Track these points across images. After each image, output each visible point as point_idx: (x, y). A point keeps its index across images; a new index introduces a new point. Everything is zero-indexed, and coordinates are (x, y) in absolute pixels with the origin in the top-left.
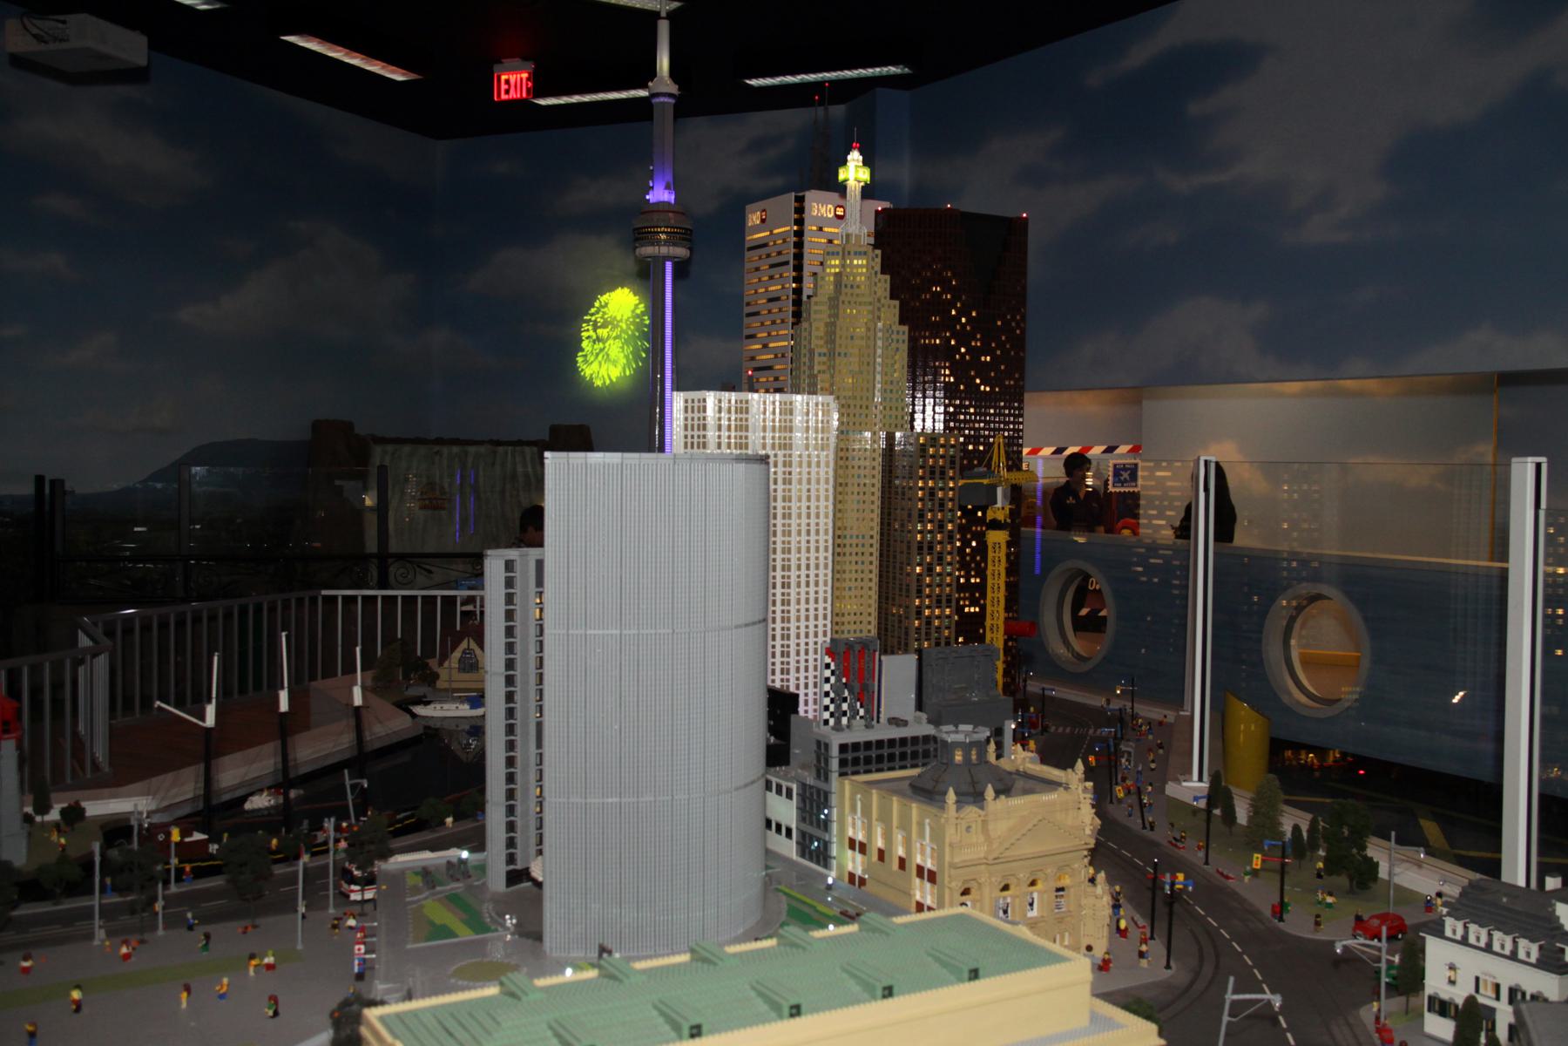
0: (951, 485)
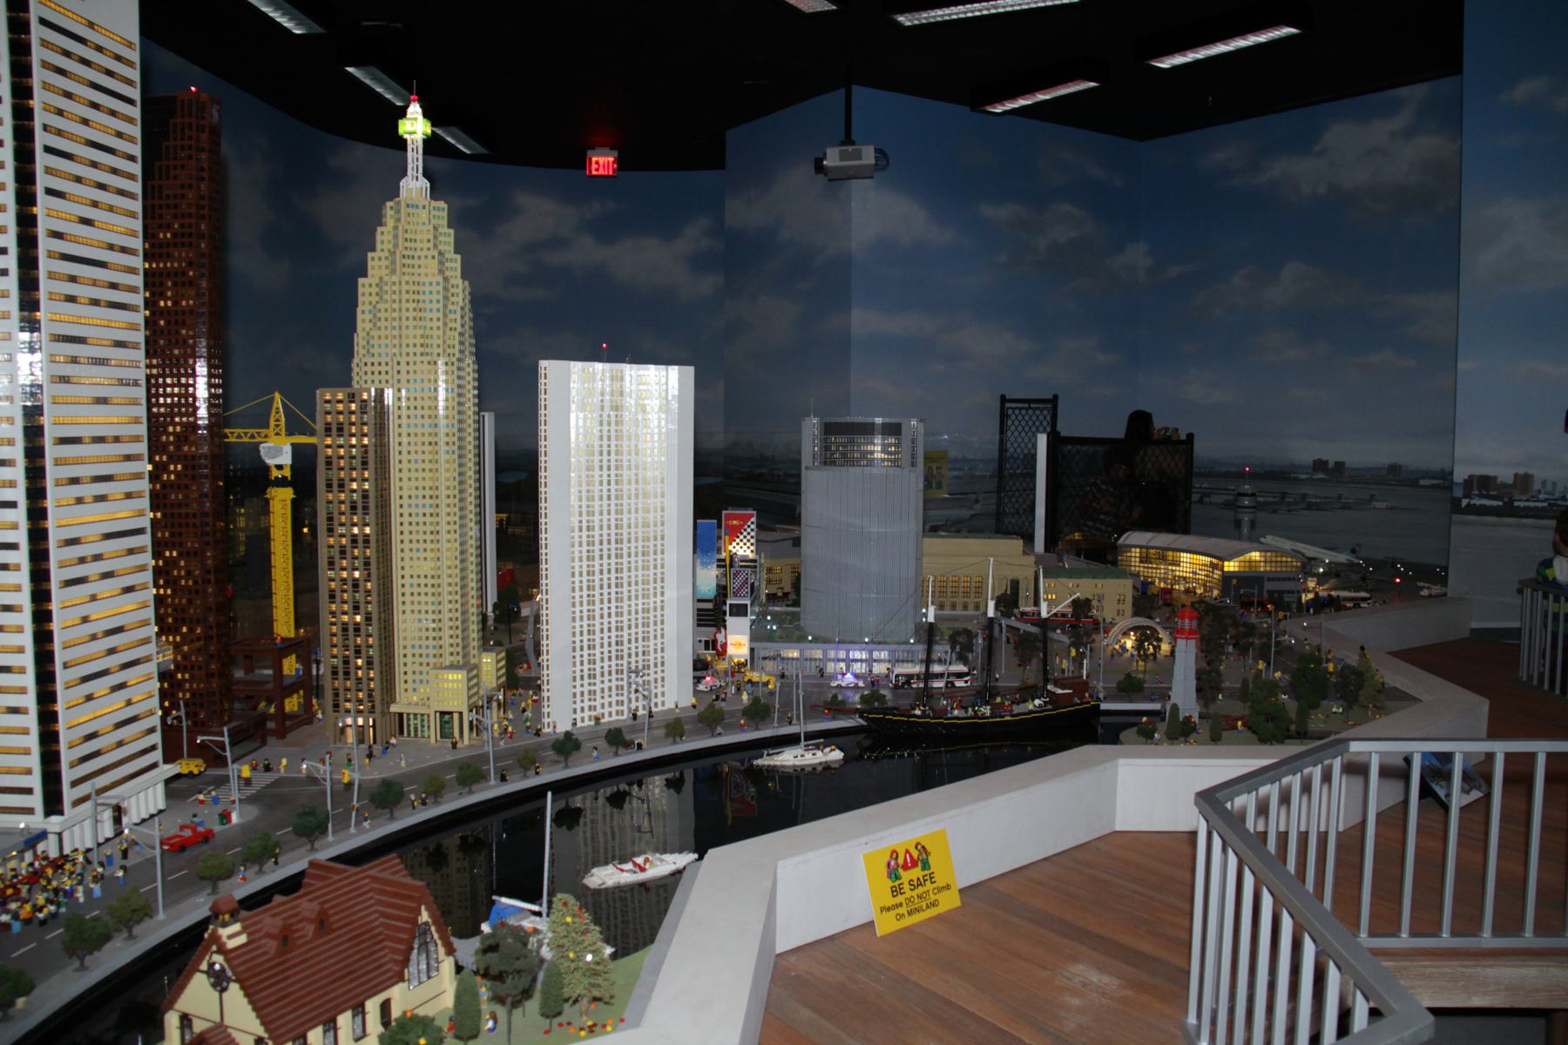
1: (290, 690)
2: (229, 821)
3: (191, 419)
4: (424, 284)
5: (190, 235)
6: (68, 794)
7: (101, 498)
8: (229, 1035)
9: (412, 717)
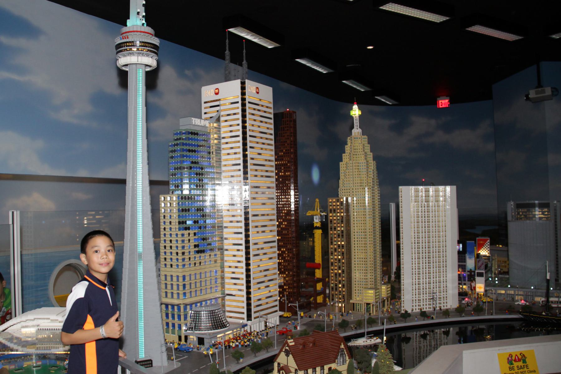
0: (339, 217)
1: (319, 294)
2: (297, 329)
3: (289, 208)
4: (360, 163)
5: (288, 153)
6: (253, 315)
7: (263, 232)
8: (289, 368)
9: (357, 305)
